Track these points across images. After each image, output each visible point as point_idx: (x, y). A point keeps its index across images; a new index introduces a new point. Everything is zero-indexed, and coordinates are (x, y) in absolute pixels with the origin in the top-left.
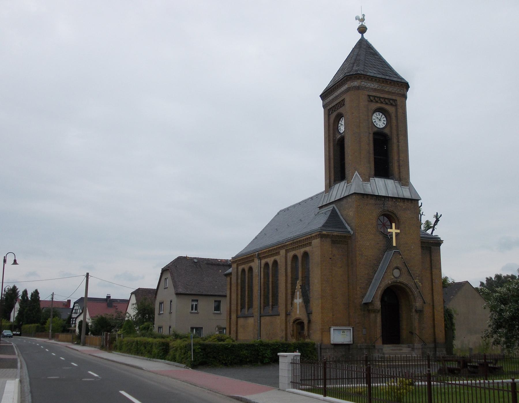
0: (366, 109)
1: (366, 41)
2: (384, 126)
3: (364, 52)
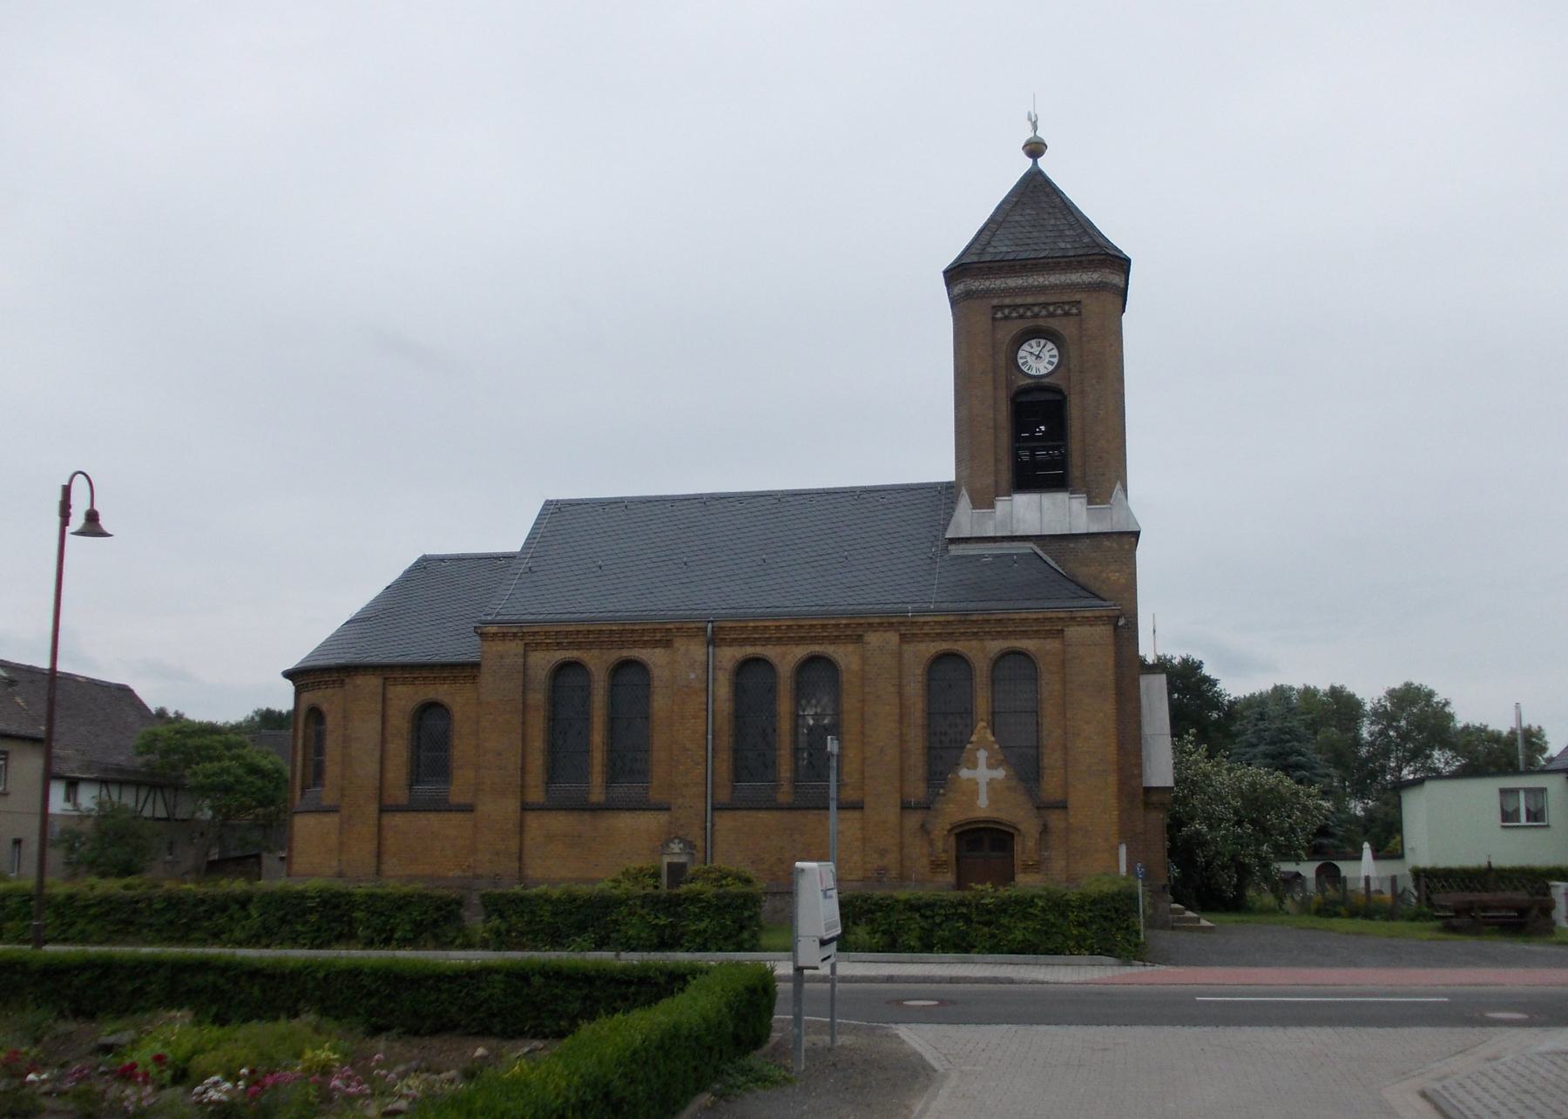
0: (1039, 302)
1: (1040, 173)
2: (1051, 368)
3: (1036, 196)
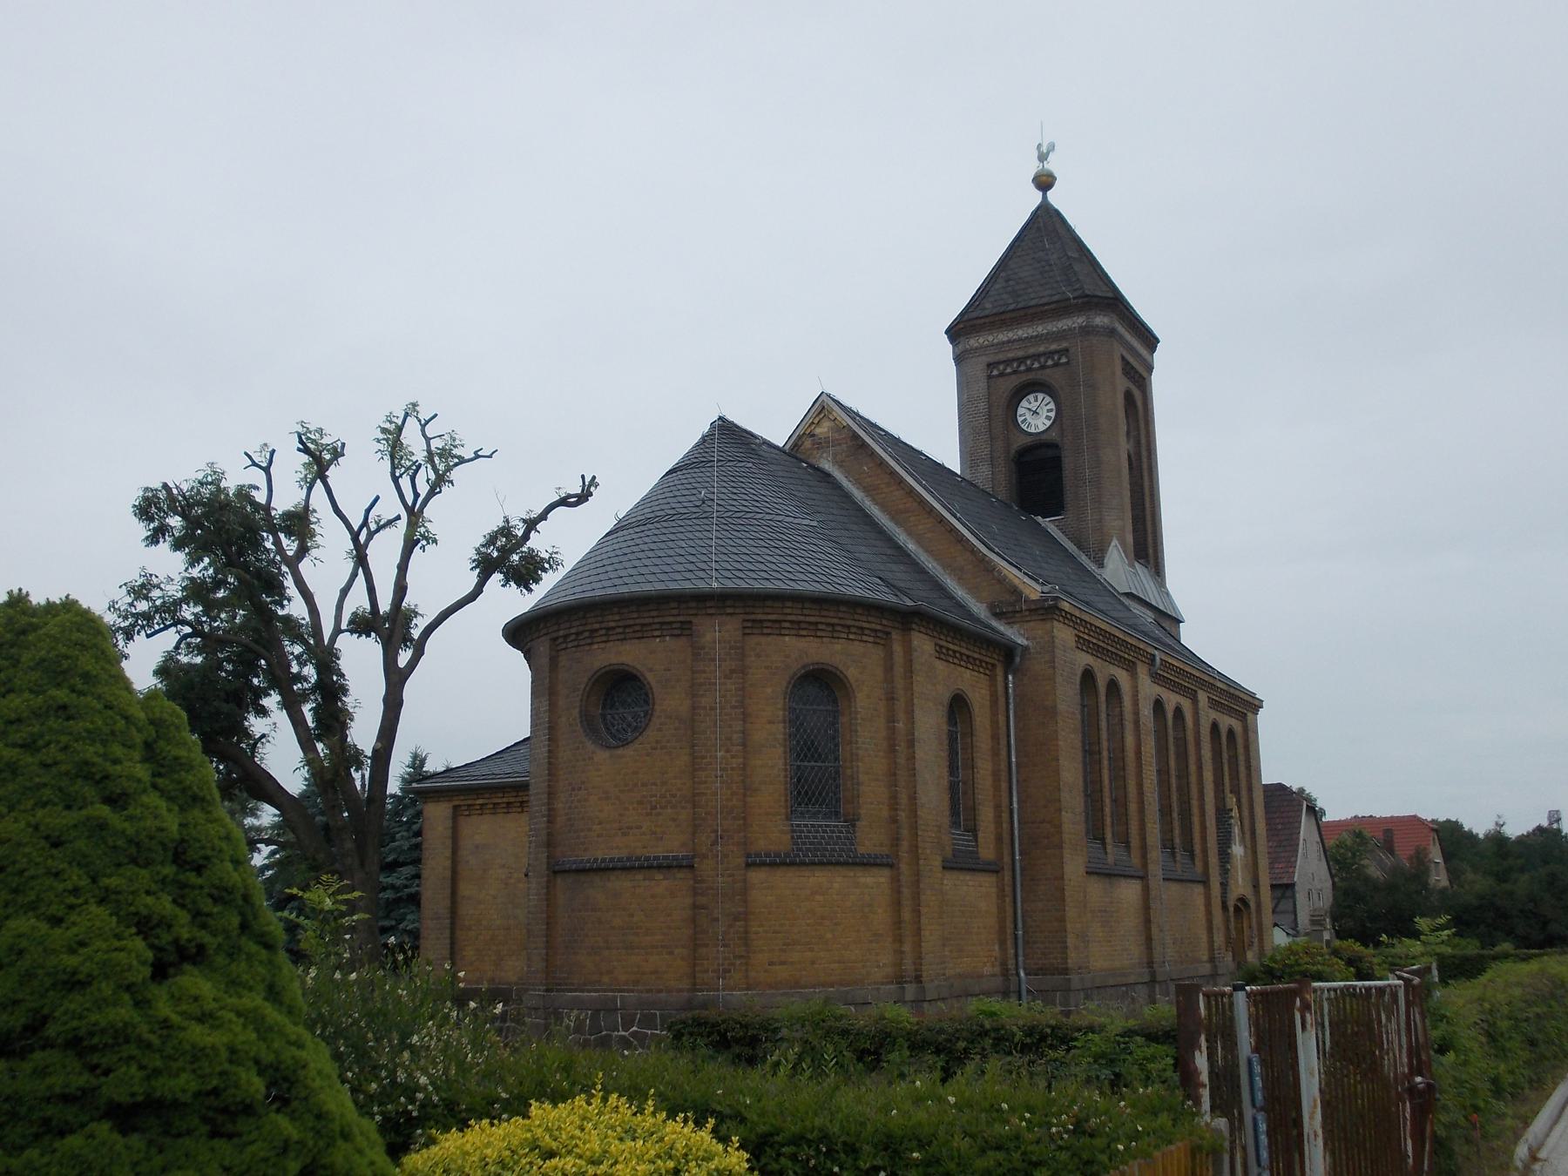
2: (1049, 423)
